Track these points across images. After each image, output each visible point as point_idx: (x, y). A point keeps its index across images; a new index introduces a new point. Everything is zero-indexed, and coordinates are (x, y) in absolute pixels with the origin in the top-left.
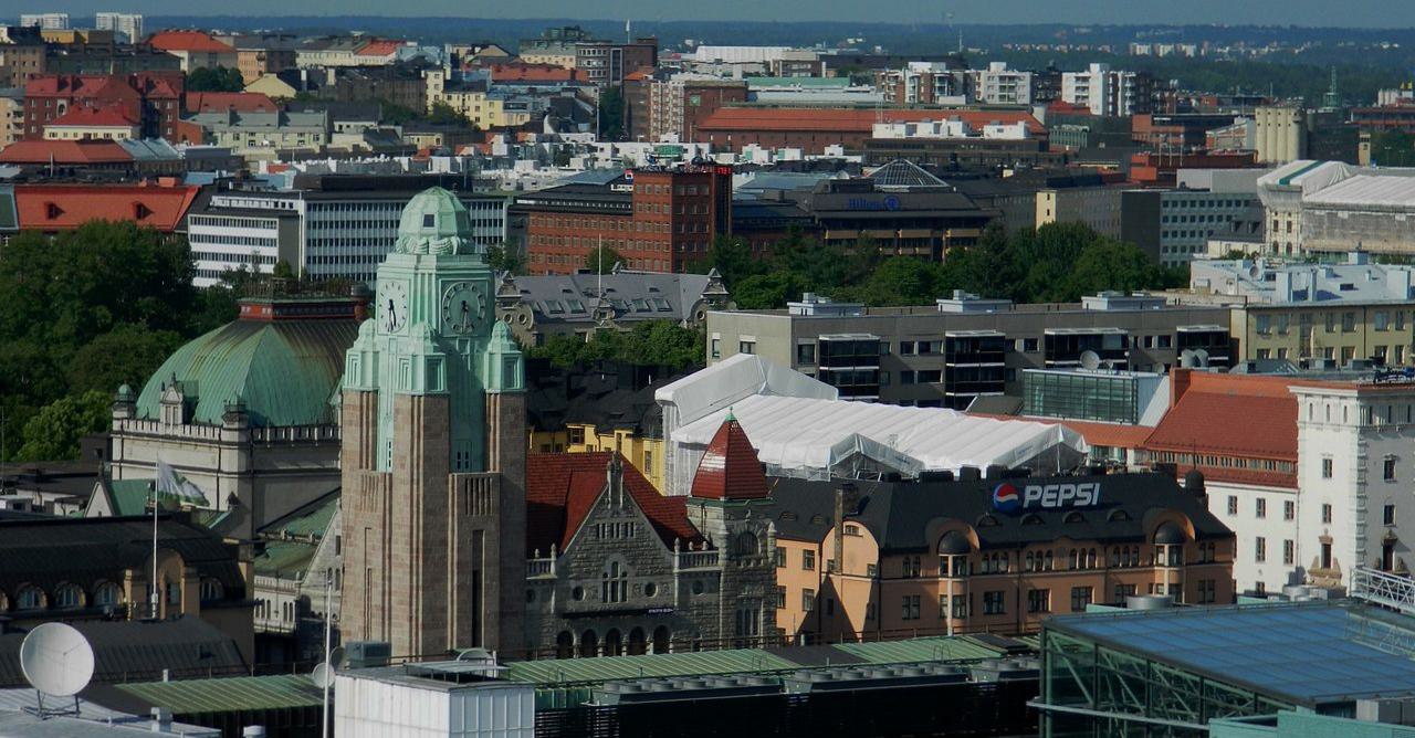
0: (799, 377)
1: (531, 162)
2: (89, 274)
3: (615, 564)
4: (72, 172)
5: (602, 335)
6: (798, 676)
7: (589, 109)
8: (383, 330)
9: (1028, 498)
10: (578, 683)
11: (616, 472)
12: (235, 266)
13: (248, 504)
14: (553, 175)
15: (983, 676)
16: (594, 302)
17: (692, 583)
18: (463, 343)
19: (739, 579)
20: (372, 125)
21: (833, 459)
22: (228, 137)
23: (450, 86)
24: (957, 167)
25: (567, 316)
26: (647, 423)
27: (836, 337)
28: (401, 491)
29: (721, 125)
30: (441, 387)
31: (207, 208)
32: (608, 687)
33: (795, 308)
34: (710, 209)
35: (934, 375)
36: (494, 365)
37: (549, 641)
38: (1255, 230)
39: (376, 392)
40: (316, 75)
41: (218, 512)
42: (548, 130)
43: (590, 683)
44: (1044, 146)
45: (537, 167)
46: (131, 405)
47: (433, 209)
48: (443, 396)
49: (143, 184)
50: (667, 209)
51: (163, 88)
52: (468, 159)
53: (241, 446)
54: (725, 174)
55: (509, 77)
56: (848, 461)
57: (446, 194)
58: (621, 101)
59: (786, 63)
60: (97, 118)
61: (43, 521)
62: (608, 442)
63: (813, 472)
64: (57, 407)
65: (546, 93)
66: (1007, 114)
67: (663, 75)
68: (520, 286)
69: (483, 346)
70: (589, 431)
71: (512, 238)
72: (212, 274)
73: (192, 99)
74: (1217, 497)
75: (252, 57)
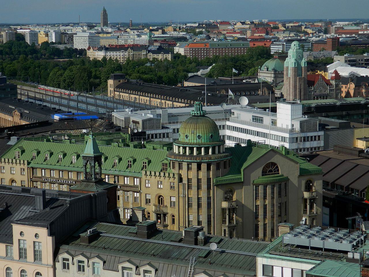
0: (345, 64)
1: (315, 37)
2: (257, 52)
3: (321, 88)
4: (257, 40)
5: (322, 59)
7: (323, 31)
10: (310, 103)
11: (321, 76)
12: (276, 51)
14: (318, 39)
16: (321, 55)
17: (331, 90)
18: (299, 61)
19: (336, 90)
21: (349, 74)
22: (277, 35)
23: (305, 28)
26: (326, 70)
27: (350, 59)
28: (291, 79)
31: (273, 44)
32: (314, 104)
33: (345, 55)
34: (337, 43)
35: (363, 64)
36: (303, 63)
37: (312, 98)
40: (288, 27)
42: (317, 33)
43: (311, 103)
46: (260, 69)
48: (296, 67)
50: (331, 43)
51: (269, 29)
52: (307, 37)
53: (274, 74)
54: (339, 38)
55: (312, 27)
58: (327, 29)
60: (261, 33)
61: (250, 83)
62: (321, 73)
63: (347, 76)
64: (253, 69)
65: (317, 28)
67: (332, 26)
68: (312, 53)
70: (319, 71)
71: (311, 47)
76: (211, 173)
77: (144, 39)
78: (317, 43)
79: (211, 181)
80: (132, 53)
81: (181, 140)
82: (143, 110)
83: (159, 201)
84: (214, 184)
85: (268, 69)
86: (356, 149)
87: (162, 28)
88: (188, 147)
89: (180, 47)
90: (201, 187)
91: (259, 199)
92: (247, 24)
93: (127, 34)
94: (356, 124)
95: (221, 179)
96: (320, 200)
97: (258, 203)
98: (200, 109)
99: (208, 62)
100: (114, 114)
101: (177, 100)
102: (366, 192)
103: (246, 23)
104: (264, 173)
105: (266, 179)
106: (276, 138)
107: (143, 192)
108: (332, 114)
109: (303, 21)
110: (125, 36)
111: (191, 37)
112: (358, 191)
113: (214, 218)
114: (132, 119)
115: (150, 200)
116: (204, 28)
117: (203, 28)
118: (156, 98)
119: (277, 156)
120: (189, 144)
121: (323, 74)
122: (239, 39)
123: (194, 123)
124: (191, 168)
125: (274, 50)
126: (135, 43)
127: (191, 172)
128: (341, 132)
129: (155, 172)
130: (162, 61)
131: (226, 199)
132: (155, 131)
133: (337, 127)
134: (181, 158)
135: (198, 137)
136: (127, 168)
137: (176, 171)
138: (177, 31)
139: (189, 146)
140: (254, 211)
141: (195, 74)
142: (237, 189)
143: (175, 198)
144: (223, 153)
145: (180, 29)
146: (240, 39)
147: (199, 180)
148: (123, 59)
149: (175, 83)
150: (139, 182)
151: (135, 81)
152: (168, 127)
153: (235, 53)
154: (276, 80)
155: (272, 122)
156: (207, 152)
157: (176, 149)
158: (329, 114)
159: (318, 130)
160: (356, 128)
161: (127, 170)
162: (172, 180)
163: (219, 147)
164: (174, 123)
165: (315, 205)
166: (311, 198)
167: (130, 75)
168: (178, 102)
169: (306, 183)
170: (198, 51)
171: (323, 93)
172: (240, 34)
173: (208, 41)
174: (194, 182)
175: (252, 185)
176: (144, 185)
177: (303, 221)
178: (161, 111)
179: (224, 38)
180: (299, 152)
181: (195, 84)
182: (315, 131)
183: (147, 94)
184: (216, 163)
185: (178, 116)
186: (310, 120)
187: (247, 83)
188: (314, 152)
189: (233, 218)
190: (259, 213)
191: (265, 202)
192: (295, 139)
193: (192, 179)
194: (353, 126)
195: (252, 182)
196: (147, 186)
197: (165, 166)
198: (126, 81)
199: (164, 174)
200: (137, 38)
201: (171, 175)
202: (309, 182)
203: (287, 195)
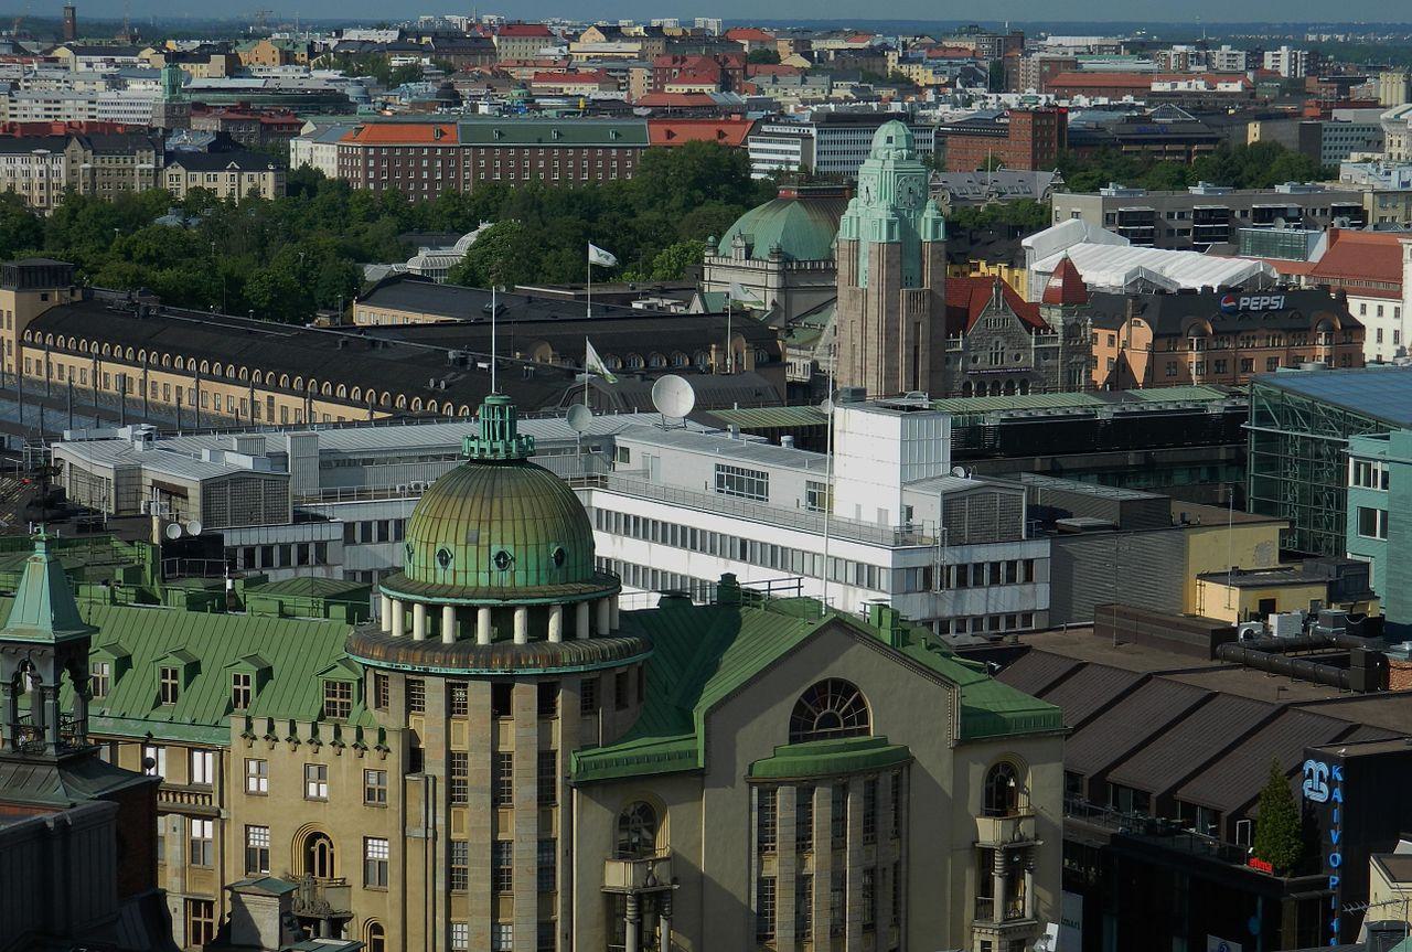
0: (1106, 232)
3: (997, 342)
4: (681, 112)
5: (990, 207)
6: (1105, 409)
7: (983, 74)
9: (1242, 304)
10: (976, 412)
11: (999, 288)
12: (775, 167)
14: (961, 113)
15: (1215, 409)
16: (986, 188)
17: (1043, 354)
18: (909, 212)
19: (1069, 352)
21: (1126, 281)
23: (901, 60)
24: (1201, 108)
25: (970, 196)
26: (1017, 259)
28: (873, 300)
29: (1061, 83)
30: (896, 238)
31: (759, 133)
32: (993, 415)
33: (1104, 192)
34: (1055, 133)
35: (1186, 232)
36: (928, 225)
38: (1379, 145)
40: (823, 54)
41: (766, 311)
42: (959, 86)
44: (1253, 96)
46: (715, 248)
47: (892, 133)
48: (895, 243)
49: (722, 119)
50: (1029, 133)
51: (734, 62)
54: (1063, 113)
55: (935, 53)
56: (1135, 282)
58: (1002, 69)
61: (661, 315)
62: (994, 271)
63: (1114, 288)
64: (674, 249)
66: (1232, 76)
67: (1027, 54)
70: (983, 264)
71: (937, 150)
73: (751, 68)
74: (1354, 305)
75: (786, 44)
76: (557, 727)
77: (144, 97)
78: (964, 134)
79: (554, 764)
80: (87, 166)
81: (417, 575)
82: (200, 434)
83: (309, 857)
84: (569, 778)
86: (1197, 624)
87: (223, 49)
88: (451, 605)
89: (315, 137)
90: (510, 792)
91: (773, 848)
92: (629, 39)
93: (60, 74)
94: (1193, 511)
95: (602, 757)
96: (1052, 860)
97: (773, 868)
98: (507, 431)
99: (455, 215)
100: (59, 451)
101: (327, 388)
102: (1254, 822)
103: (623, 30)
104: (800, 728)
105: (809, 758)
106: (836, 569)
107: (232, 818)
108: (1077, 461)
109: (889, 28)
110: (49, 82)
111: (366, 92)
112: (1215, 815)
113: (568, 936)
114: (151, 473)
115: (264, 852)
116: (424, 52)
117: (423, 50)
118: (223, 379)
119: (858, 649)
120: (455, 592)
121: (1005, 275)
122: (595, 107)
123: (479, 493)
124: (465, 705)
126: (95, 117)
127: (466, 723)
128: (1128, 544)
129: (271, 721)
130: (232, 205)
131: (624, 852)
132: (263, 532)
133: (1109, 522)
134: (418, 659)
135: (498, 558)
136: (157, 704)
137: (392, 718)
138: (296, 63)
139: (452, 600)
140: (754, 907)
141: (396, 268)
142: (673, 804)
143: (386, 843)
144: (613, 634)
145: (312, 53)
147: (500, 763)
148: (44, 193)
149: (303, 309)
150: (214, 770)
151: (121, 296)
152: (321, 512)
153: (578, 171)
155: (812, 497)
156: (537, 629)
157: (389, 615)
158: (1066, 461)
159: (1023, 537)
160: (1194, 526)
161: (155, 713)
162: (371, 759)
163: (594, 606)
164: (347, 495)
165: (1028, 877)
166: (1013, 846)
167: (92, 272)
168: (334, 399)
169: (992, 774)
170: (405, 159)
171: (1012, 365)
172: (597, 86)
173: (449, 113)
174: (478, 770)
175: (742, 785)
176: (236, 785)
177: (1049, 937)
178: (289, 438)
179: (526, 102)
181: (408, 314)
182: (1012, 537)
183: (179, 362)
184: (580, 682)
185: (365, 462)
186: (986, 490)
187: (652, 315)
188: (1006, 634)
189: (653, 937)
190: (773, 913)
191: (802, 863)
192: (920, 574)
193: (465, 756)
194: (1183, 515)
195: (741, 770)
196: (253, 786)
197: (342, 697)
198: (78, 296)
199: (338, 733)
200: (104, 93)
201: (371, 738)
202: (1001, 773)
203: (904, 830)
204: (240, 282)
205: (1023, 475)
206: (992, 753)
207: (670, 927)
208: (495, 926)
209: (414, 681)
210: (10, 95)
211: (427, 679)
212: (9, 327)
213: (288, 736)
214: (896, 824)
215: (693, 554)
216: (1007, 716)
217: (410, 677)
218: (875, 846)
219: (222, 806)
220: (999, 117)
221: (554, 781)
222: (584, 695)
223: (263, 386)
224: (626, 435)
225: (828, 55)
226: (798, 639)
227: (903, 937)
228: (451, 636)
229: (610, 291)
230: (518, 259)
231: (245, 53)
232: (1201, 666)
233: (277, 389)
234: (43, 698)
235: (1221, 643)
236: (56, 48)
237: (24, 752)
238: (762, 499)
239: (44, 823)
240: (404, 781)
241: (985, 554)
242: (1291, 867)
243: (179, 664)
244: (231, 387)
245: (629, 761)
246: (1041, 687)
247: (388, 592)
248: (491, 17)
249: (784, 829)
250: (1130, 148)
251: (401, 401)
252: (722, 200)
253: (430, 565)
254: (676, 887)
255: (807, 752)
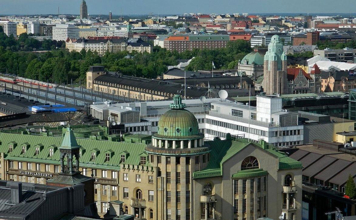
0: (325, 58)
1: (295, 31)
3: (301, 82)
5: (302, 53)
6: (318, 97)
8: (269, 53)
9: (354, 74)
11: (301, 70)
12: (256, 45)
13: (255, 74)
14: (298, 33)
15: (342, 97)
17: (311, 84)
18: (279, 54)
19: (316, 84)
20: (275, 27)
22: (257, 28)
23: (285, 22)
24: (349, 31)
25: (298, 50)
26: (306, 64)
28: (271, 73)
29: (320, 26)
30: (276, 60)
31: (253, 37)
32: (293, 98)
33: (325, 50)
34: (317, 37)
35: (343, 58)
36: (283, 57)
37: (292, 92)
39: (268, 60)
40: (268, 21)
41: (251, 76)
42: (297, 27)
45: (296, 32)
46: (240, 62)
49: (246, 34)
50: (311, 37)
51: (249, 22)
54: (319, 33)
55: (293, 21)
56: (331, 69)
57: (277, 35)
59: (328, 18)
61: (229, 77)
62: (301, 67)
63: (326, 70)
64: (233, 62)
67: (312, 20)
69: (281, 55)
70: (299, 65)
71: (292, 41)
72: (253, 46)
73: (253, 24)
75: (261, 19)
76: (190, 166)
77: (124, 31)
79: (189, 174)
83: (137, 194)
85: (247, 63)
87: (141, 21)
89: (159, 39)
91: (238, 193)
93: (107, 27)
96: (299, 195)
97: (238, 197)
98: (179, 102)
99: (188, 55)
100: (92, 106)
101: (156, 93)
104: (243, 167)
105: (245, 173)
106: (256, 132)
107: (121, 186)
108: (311, 108)
111: (171, 29)
112: (337, 186)
113: (192, 212)
114: (111, 111)
115: (127, 193)
117: (183, 21)
118: (135, 91)
120: (168, 137)
122: (219, 32)
124: (170, 162)
125: (254, 43)
127: (180, 166)
128: (320, 126)
130: (141, 54)
131: (205, 193)
132: (134, 124)
134: (160, 152)
136: (105, 161)
137: (154, 164)
138: (157, 24)
139: (167, 139)
140: (233, 206)
141: (175, 67)
143: (153, 192)
144: (202, 146)
145: (160, 21)
146: (220, 32)
147: (178, 174)
148: (102, 52)
149: (155, 77)
152: (147, 120)
154: (256, 74)
155: (252, 116)
157: (154, 142)
159: (298, 125)
160: (335, 122)
162: (150, 173)
164: (153, 116)
165: (294, 199)
168: (157, 95)
170: (178, 44)
171: (303, 87)
172: (220, 28)
173: (188, 34)
175: (231, 179)
177: (282, 215)
178: (140, 104)
179: (204, 31)
180: (278, 146)
181: (175, 76)
185: (157, 109)
186: (290, 114)
189: (211, 212)
191: (244, 196)
192: (275, 133)
193: (170, 173)
194: (333, 120)
196: (125, 179)
198: (105, 73)
199: (143, 168)
200: (116, 31)
201: (150, 169)
204: (141, 70)
205: (299, 111)
206: (286, 172)
207: (215, 210)
208: (177, 209)
209: (159, 157)
210: (97, 31)
211: (162, 156)
212: (91, 80)
213: (142, 169)
214: (265, 188)
215: (227, 128)
216: (290, 164)
217: (158, 156)
218: (260, 193)
219: (118, 183)
220: (305, 34)
221: (189, 178)
222: (196, 160)
223: (143, 92)
224: (213, 103)
225: (269, 21)
226: (242, 148)
227: (266, 213)
228: (175, 147)
229: (218, 71)
230: (200, 65)
231: (146, 22)
232: (336, 153)
233: (146, 93)
234: (69, 161)
235: (340, 148)
236: (106, 21)
237: (65, 173)
238: (242, 117)
239: (68, 188)
240: (157, 178)
241: (289, 128)
242: (353, 197)
243: (110, 153)
244: (136, 92)
245: (206, 174)
246: (299, 159)
247: (154, 137)
248: (199, 14)
249: (240, 189)
250: (333, 40)
251: (171, 95)
252: (245, 52)
253: (163, 131)
254: (216, 201)
255: (245, 172)
